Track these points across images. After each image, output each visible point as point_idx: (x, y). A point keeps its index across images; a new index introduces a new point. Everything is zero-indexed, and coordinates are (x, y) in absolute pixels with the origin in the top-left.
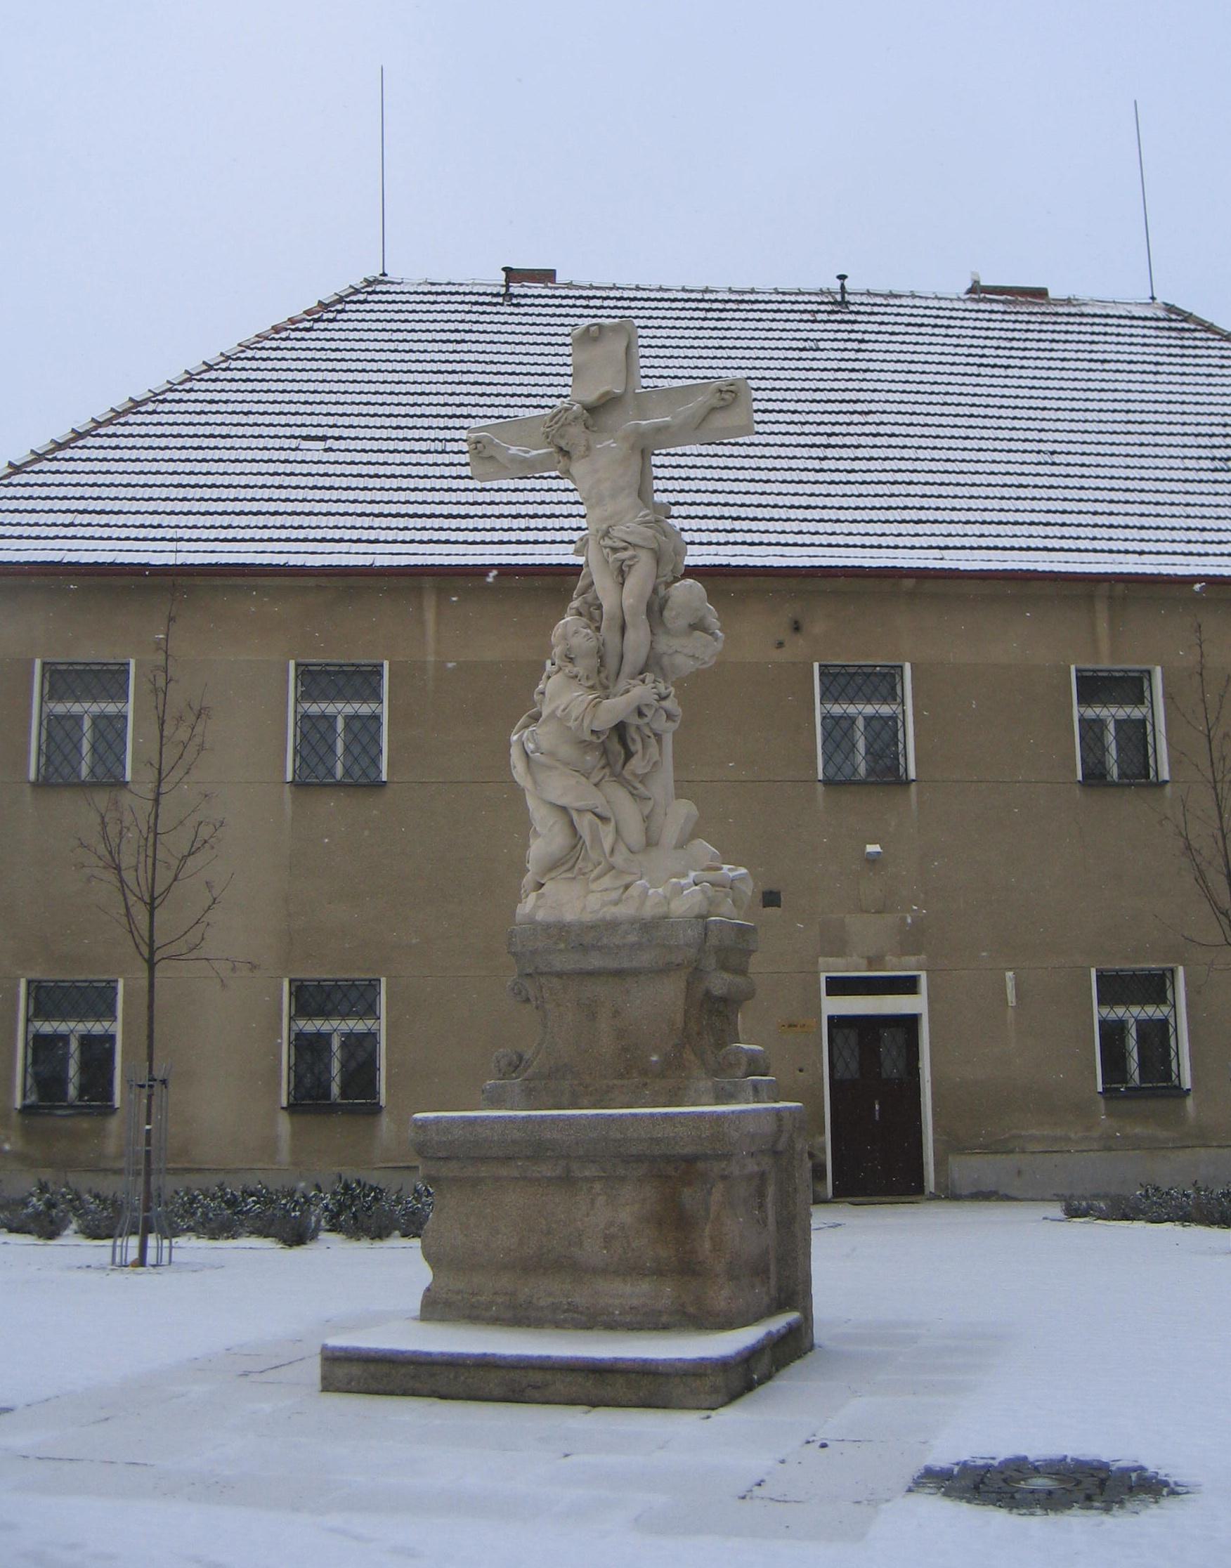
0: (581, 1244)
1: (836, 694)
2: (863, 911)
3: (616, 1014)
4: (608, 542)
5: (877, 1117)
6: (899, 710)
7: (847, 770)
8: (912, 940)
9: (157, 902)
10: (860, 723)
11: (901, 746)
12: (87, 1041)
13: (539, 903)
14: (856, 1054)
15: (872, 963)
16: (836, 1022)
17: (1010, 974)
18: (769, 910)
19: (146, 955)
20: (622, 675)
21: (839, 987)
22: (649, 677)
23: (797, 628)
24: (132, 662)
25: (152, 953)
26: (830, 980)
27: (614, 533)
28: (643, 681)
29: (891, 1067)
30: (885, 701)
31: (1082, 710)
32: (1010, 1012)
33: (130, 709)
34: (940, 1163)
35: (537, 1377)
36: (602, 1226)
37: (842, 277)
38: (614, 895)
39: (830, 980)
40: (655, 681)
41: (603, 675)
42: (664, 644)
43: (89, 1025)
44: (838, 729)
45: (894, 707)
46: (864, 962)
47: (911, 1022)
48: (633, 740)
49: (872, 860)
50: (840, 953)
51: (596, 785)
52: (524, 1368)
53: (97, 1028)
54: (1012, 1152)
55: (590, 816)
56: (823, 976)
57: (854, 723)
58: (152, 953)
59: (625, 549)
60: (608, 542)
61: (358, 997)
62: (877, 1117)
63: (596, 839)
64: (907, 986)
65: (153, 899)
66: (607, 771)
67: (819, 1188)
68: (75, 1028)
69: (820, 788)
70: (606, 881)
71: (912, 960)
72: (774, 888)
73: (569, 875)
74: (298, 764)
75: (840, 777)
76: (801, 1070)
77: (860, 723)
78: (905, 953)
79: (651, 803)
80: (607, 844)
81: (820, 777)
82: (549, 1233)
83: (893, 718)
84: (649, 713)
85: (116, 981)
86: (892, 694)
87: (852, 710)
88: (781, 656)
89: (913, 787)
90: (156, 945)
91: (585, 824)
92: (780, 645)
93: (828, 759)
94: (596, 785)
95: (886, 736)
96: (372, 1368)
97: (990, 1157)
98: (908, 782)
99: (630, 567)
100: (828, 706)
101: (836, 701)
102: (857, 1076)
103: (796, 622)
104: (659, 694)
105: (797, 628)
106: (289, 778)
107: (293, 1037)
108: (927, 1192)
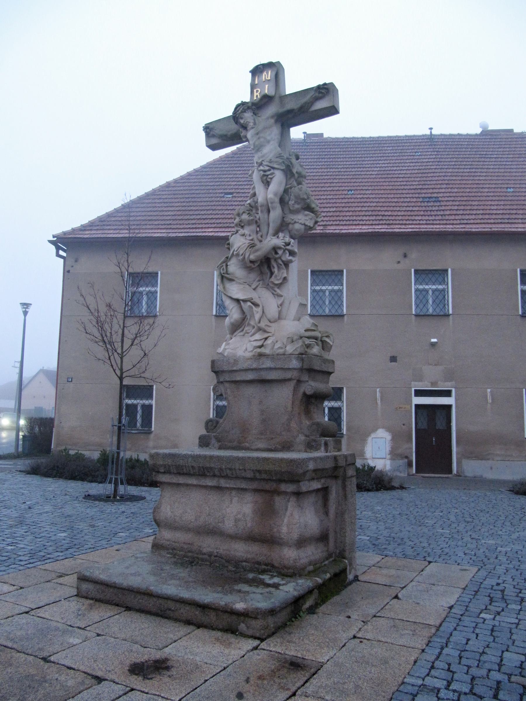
0: (223, 522)
1: (421, 281)
2: (430, 364)
3: (261, 402)
4: (261, 168)
5: (434, 444)
6: (446, 287)
7: (424, 310)
8: (449, 376)
9: (124, 354)
10: (430, 292)
11: (446, 302)
12: (143, 406)
13: (226, 347)
14: (426, 419)
15: (433, 384)
16: (417, 406)
17: (489, 390)
18: (393, 363)
19: (119, 375)
20: (269, 234)
21: (419, 393)
22: (281, 235)
23: (405, 256)
24: (159, 272)
25: (122, 373)
26: (416, 391)
27: (264, 163)
28: (278, 237)
29: (440, 425)
30: (440, 284)
31: (522, 287)
32: (489, 405)
33: (158, 289)
34: (459, 463)
35: (171, 605)
36: (235, 514)
37: (431, 129)
38: (259, 343)
39: (416, 391)
40: (284, 237)
41: (259, 235)
42: (291, 217)
43: (144, 401)
44: (421, 294)
45: (444, 286)
46: (429, 384)
47: (449, 407)
48: (274, 267)
49: (433, 345)
50: (421, 380)
51: (254, 289)
52: (165, 598)
53: (147, 402)
54: (488, 459)
55: (249, 304)
56: (413, 389)
57: (428, 292)
58: (122, 373)
59: (269, 170)
60: (261, 168)
61: (146, 391)
62: (434, 444)
63: (252, 316)
64: (447, 393)
65: (123, 352)
66: (261, 282)
67: (410, 470)
68: (139, 402)
69: (413, 317)
70: (258, 336)
71: (449, 384)
72: (395, 355)
73: (242, 334)
74: (218, 308)
75: (422, 313)
76: (404, 425)
77: (430, 292)
78: (446, 381)
79: (283, 298)
80: (257, 317)
81: (414, 313)
82: (209, 515)
83: (443, 290)
84: (280, 252)
85: (153, 386)
86: (444, 281)
87: (427, 287)
88: (400, 266)
89: (451, 317)
90: (124, 371)
91: (246, 306)
92: (399, 262)
93: (417, 306)
94: (254, 289)
95: (441, 297)
96: (98, 587)
97: (480, 461)
98: (448, 315)
99: (271, 179)
100: (417, 286)
101: (421, 284)
102: (427, 428)
103: (405, 254)
104: (285, 243)
105: (405, 256)
106: (214, 313)
107: (215, 407)
108: (453, 473)
